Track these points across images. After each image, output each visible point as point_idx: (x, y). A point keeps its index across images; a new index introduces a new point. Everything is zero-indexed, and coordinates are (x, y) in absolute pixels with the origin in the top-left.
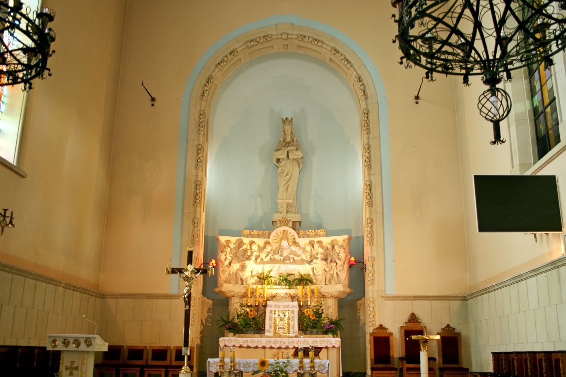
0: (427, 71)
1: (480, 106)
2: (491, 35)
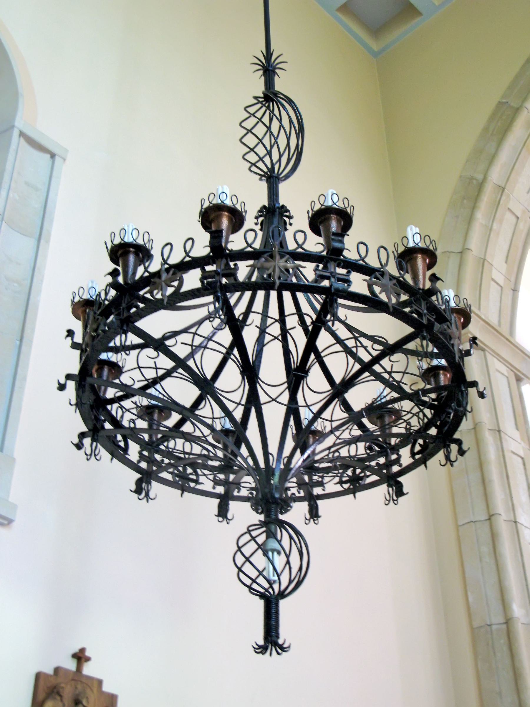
0: (139, 476)
1: (240, 560)
2: (274, 400)
